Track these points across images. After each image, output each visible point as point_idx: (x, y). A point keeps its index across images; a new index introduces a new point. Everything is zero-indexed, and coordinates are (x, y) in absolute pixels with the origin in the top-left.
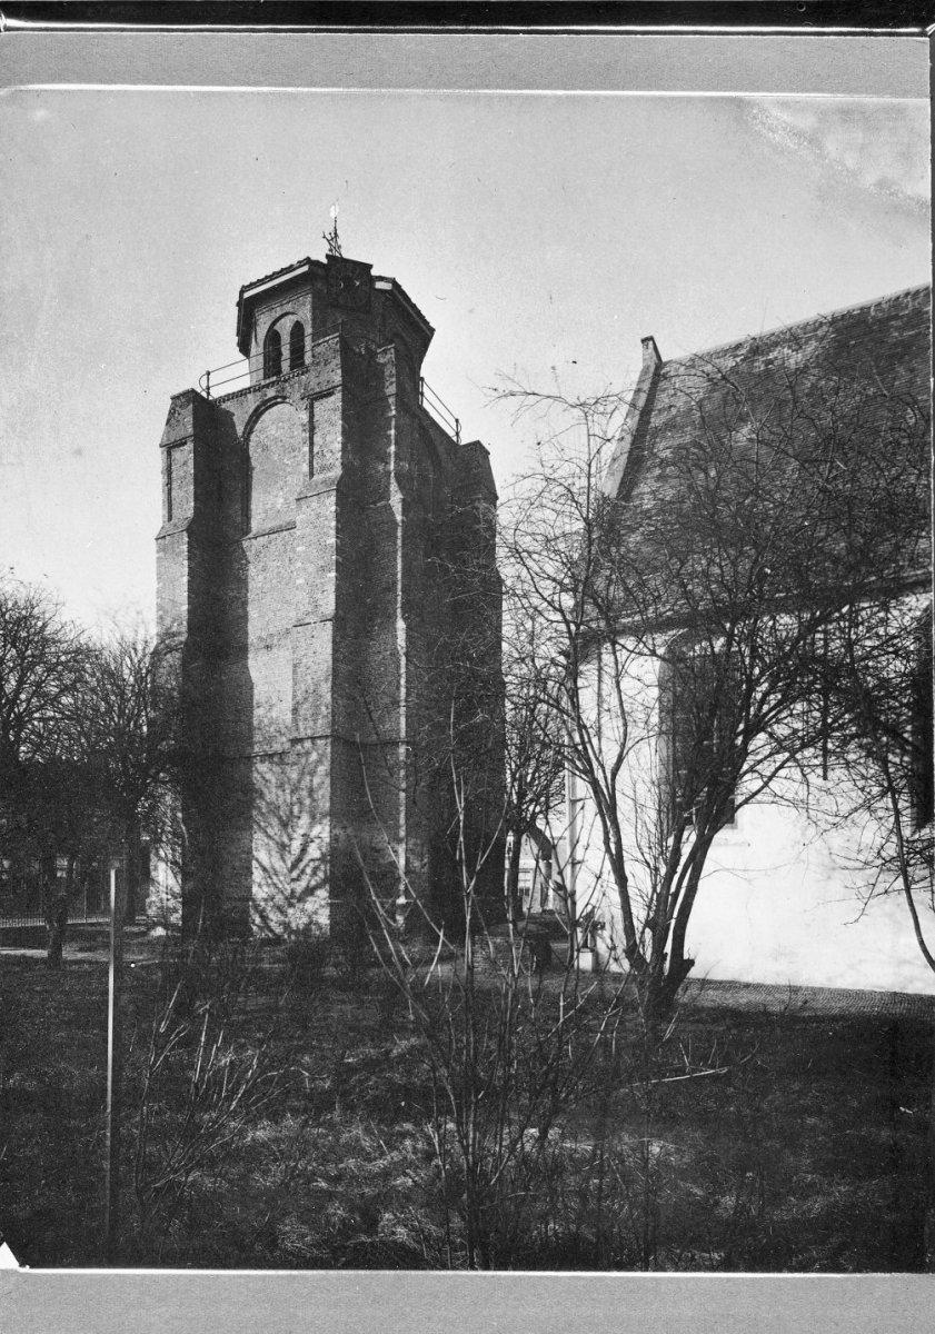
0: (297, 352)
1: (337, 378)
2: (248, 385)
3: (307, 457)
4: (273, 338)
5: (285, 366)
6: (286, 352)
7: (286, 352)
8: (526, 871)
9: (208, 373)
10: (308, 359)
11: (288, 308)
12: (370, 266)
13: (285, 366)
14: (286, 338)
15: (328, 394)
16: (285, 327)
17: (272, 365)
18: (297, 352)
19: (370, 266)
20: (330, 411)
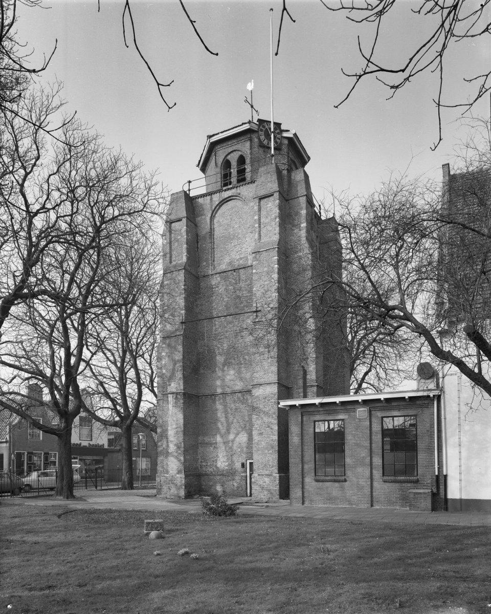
0: (241, 172)
1: (184, 214)
2: (205, 192)
3: (257, 230)
4: (227, 164)
5: (234, 180)
6: (234, 171)
7: (234, 171)
8: (150, 342)
9: (190, 182)
10: (248, 175)
11: (234, 148)
12: (281, 124)
13: (234, 180)
14: (234, 164)
15: (180, 220)
16: (234, 159)
17: (226, 180)
18: (241, 172)
19: (281, 124)
20: (272, 206)
